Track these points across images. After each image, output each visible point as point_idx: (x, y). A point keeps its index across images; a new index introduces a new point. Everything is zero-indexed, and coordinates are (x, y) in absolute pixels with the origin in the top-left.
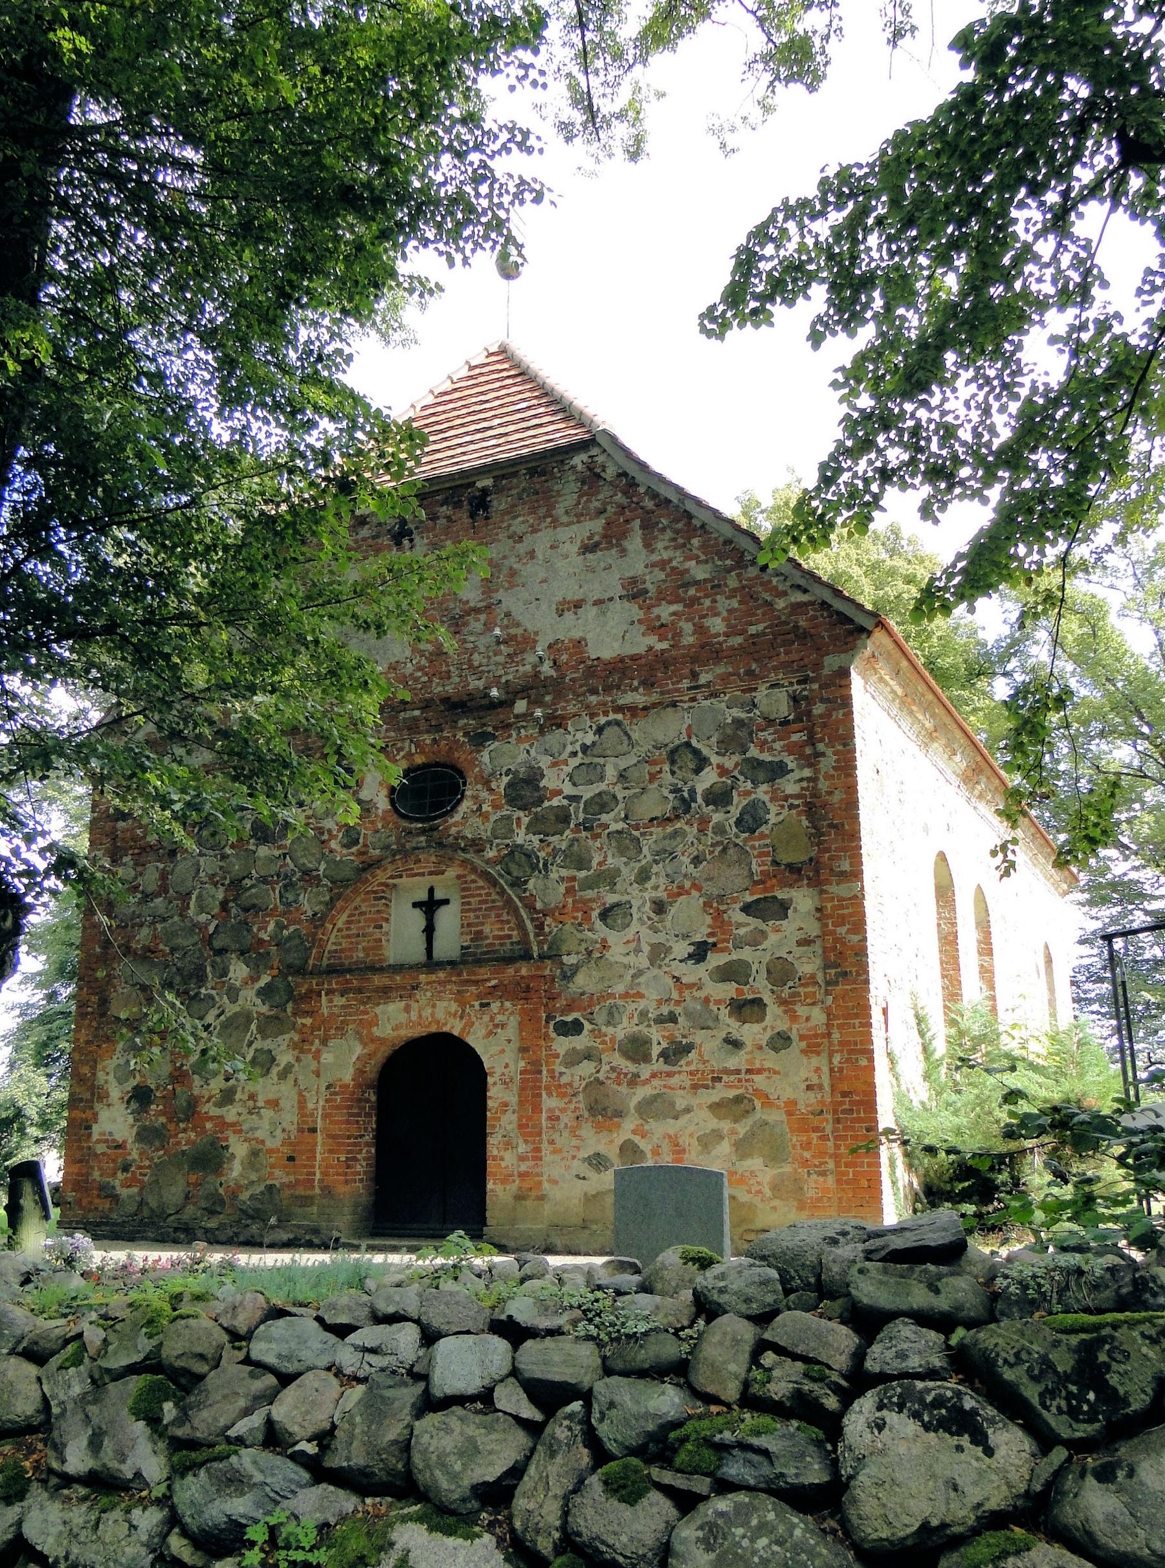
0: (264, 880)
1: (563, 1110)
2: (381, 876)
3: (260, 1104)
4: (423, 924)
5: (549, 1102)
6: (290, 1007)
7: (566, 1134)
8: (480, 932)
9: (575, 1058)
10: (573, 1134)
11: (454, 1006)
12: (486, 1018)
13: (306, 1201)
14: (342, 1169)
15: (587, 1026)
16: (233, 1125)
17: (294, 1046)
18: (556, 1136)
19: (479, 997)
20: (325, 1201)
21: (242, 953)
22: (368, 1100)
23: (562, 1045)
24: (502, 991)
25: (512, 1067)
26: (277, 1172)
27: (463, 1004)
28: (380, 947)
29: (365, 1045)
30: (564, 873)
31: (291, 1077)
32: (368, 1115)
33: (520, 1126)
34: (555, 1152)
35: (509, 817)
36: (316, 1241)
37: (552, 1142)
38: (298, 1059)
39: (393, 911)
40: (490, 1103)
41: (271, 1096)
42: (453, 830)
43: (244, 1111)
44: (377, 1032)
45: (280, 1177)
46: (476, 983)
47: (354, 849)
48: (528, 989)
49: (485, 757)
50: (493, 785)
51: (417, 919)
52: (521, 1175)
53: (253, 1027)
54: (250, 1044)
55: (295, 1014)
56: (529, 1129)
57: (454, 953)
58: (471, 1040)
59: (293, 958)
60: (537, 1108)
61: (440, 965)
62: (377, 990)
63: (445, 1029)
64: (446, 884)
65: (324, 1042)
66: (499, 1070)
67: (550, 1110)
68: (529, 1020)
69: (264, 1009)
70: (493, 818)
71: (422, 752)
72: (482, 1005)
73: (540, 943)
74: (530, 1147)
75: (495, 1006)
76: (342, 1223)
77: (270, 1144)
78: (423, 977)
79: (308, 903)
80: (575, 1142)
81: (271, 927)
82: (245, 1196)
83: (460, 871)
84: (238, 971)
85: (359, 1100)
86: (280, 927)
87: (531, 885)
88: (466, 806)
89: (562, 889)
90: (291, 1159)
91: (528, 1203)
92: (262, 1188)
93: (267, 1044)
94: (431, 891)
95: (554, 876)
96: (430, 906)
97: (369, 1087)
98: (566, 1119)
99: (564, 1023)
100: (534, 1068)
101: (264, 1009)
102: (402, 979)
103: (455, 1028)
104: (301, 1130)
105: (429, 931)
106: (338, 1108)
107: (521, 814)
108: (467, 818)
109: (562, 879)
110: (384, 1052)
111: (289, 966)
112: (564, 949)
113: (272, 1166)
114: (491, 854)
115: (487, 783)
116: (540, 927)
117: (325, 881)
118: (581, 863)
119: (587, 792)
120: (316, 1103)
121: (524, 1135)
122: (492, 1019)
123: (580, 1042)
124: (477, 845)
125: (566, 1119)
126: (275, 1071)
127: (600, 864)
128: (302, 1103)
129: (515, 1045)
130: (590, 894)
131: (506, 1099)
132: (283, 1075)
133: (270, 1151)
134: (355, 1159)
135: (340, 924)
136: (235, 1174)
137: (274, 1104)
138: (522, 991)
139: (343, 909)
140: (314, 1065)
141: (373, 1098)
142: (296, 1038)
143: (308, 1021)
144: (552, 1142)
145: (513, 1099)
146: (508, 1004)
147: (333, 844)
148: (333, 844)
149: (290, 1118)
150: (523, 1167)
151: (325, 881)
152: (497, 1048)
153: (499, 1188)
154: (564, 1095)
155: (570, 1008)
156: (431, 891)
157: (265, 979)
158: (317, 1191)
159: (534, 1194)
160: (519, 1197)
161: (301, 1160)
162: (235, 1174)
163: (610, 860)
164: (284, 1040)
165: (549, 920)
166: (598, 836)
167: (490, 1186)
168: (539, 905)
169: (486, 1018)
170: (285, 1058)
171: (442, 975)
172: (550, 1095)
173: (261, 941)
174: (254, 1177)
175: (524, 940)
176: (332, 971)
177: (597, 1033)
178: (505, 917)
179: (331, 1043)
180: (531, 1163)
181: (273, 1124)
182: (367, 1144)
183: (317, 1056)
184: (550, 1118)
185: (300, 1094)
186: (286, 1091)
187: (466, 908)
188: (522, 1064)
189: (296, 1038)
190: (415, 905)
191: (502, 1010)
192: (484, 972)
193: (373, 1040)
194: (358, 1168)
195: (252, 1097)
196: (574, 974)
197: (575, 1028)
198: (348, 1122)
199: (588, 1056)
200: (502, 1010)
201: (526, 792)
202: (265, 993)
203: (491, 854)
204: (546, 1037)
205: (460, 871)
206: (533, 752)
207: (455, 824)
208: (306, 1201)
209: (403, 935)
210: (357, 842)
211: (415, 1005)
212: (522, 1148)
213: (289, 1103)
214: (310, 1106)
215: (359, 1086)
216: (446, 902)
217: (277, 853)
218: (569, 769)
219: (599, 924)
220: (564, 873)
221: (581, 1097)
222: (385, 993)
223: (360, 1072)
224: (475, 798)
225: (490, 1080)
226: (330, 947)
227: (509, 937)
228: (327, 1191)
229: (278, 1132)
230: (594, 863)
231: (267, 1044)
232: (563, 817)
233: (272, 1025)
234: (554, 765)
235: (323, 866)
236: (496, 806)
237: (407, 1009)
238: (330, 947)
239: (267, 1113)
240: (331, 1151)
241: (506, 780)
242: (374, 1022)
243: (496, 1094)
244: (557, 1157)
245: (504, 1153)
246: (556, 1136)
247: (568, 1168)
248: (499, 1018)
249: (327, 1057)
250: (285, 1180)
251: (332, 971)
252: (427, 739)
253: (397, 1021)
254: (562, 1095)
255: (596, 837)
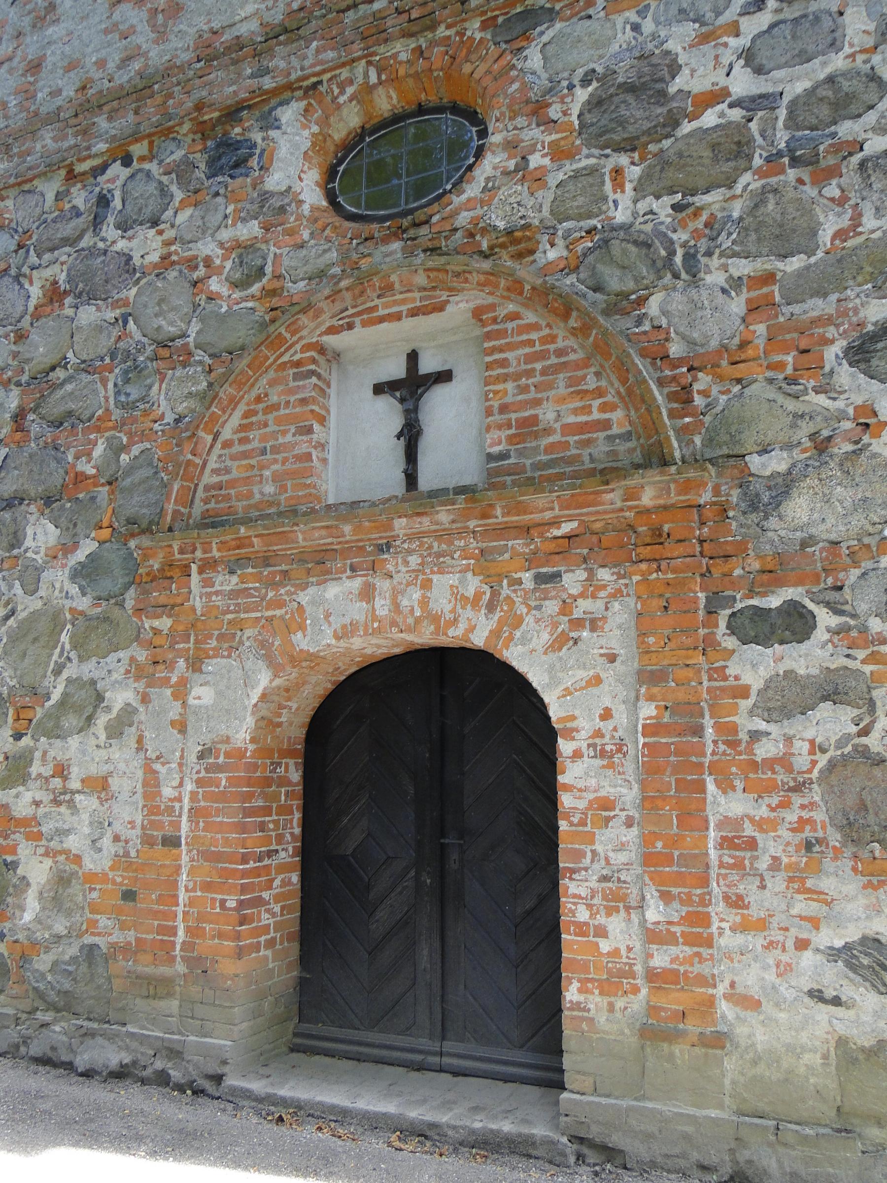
0: (87, 367)
1: (761, 825)
2: (311, 330)
3: (75, 784)
4: (396, 423)
5: (726, 804)
6: (131, 598)
7: (777, 883)
8: (534, 420)
9: (790, 699)
10: (797, 880)
11: (473, 584)
12: (552, 607)
13: (158, 988)
14: (230, 917)
15: (825, 619)
16: (24, 822)
17: (136, 671)
18: (748, 888)
19: (531, 561)
20: (194, 990)
21: (48, 501)
22: (284, 781)
23: (754, 666)
24: (590, 546)
25: (621, 717)
26: (103, 921)
27: (493, 579)
28: (309, 472)
29: (276, 669)
30: (742, 268)
31: (131, 732)
32: (285, 810)
33: (649, 859)
34: (743, 927)
35: (593, 171)
36: (176, 1075)
37: (737, 902)
38: (145, 699)
39: (333, 403)
40: (566, 800)
41: (94, 770)
42: (463, 219)
43: (46, 797)
44: (302, 642)
45: (109, 932)
46: (526, 530)
47: (255, 289)
48: (658, 537)
49: (534, 59)
50: (554, 112)
51: (387, 415)
52: (652, 975)
53: (65, 638)
54: (57, 672)
55: (139, 611)
56: (672, 865)
57: (469, 472)
58: (515, 656)
59: (137, 505)
60: (693, 817)
61: (438, 495)
62: (301, 559)
63: (453, 637)
64: (443, 334)
65: (195, 665)
66: (586, 725)
67: (725, 822)
68: (661, 611)
69: (84, 603)
70: (553, 180)
71: (394, 80)
72: (540, 579)
73: (683, 432)
74: (676, 912)
75: (573, 581)
76: (224, 1037)
77: (89, 864)
78: (400, 525)
79: (170, 396)
80: (802, 906)
81: (99, 451)
82: (43, 962)
83: (482, 299)
84: (41, 534)
85: (267, 782)
86: (117, 449)
87: (653, 306)
88: (489, 165)
89: (737, 305)
90: (129, 895)
91: (679, 1050)
92: (73, 950)
93: (88, 670)
94: (413, 357)
95: (715, 278)
96: (411, 387)
97: (290, 753)
98: (774, 846)
99: (760, 613)
100: (683, 720)
101: (84, 603)
102: (358, 540)
103: (477, 631)
104: (148, 841)
105: (411, 436)
106: (222, 797)
107: (623, 160)
108: (488, 192)
109: (736, 283)
110: (316, 688)
111: (131, 521)
112: (750, 440)
113: (94, 909)
114: (552, 254)
115: (537, 111)
116: (683, 396)
117: (199, 355)
118: (789, 238)
119: (796, 83)
120: (178, 788)
121: (659, 880)
122: (566, 608)
123: (810, 657)
124: (519, 241)
125: (774, 846)
126: (102, 720)
127: (841, 235)
128: (151, 782)
129: (627, 666)
130: (817, 307)
131: (607, 791)
132: (115, 731)
133: (91, 878)
134: (259, 902)
135: (227, 433)
136: (28, 917)
137: (99, 785)
138: (642, 543)
139: (234, 402)
140: (174, 711)
141: (296, 776)
142: (142, 655)
143: (164, 623)
144: (737, 902)
145: (627, 793)
146: (604, 575)
147: (215, 285)
148: (215, 285)
149: (128, 813)
150: (661, 960)
151: (199, 355)
152: (585, 678)
153: (595, 1002)
154: (770, 788)
155: (771, 576)
156: (413, 357)
157: (87, 548)
158: (181, 968)
159: (692, 1027)
160: (655, 1032)
161: (149, 900)
162: (28, 917)
163: (869, 222)
164: (117, 663)
165: (703, 380)
166: (833, 172)
167: (571, 994)
168: (675, 349)
169: (552, 607)
170: (120, 697)
171: (444, 516)
172: (726, 786)
173: (80, 478)
174: (60, 927)
175: (650, 425)
176: (211, 522)
177: (851, 636)
178: (591, 383)
179: (210, 666)
180: (684, 951)
181: (100, 824)
182: (283, 868)
183: (181, 692)
184: (726, 843)
185: (149, 770)
186: (123, 763)
187: (494, 372)
188: (648, 710)
189: (142, 655)
190: (379, 389)
191: (591, 589)
192: (543, 505)
193: (296, 659)
194: (266, 919)
195: (61, 771)
196: (777, 503)
197: (795, 624)
198: (242, 828)
199: (832, 690)
200: (591, 589)
201: (638, 115)
202: (85, 574)
203: (552, 254)
204: (709, 645)
205: (482, 299)
206: (648, 26)
207: (469, 205)
208: (158, 988)
209: (357, 443)
210: (260, 272)
211: (383, 585)
212: (655, 913)
213: (127, 782)
214: (167, 792)
215: (264, 752)
216: (444, 377)
217: (110, 315)
218: (744, 41)
219: (846, 375)
220: (742, 268)
221: (816, 794)
222: (319, 563)
223: (267, 724)
224: (511, 146)
225: (565, 747)
226: (208, 478)
227: (606, 425)
228: (200, 967)
229: (106, 842)
230: (825, 237)
231: (88, 670)
232: (733, 147)
233: (95, 634)
234: (704, 39)
235: (194, 329)
236: (559, 154)
237: (367, 594)
238: (208, 478)
239: (87, 803)
240: (207, 887)
241: (582, 95)
242: (297, 622)
243: (579, 777)
244: (755, 941)
245: (609, 917)
246: (748, 888)
247: (785, 970)
248: (584, 606)
249: (202, 695)
250: (117, 937)
251: (211, 522)
252: (402, 49)
253: (349, 620)
254: (761, 790)
255: (823, 176)
